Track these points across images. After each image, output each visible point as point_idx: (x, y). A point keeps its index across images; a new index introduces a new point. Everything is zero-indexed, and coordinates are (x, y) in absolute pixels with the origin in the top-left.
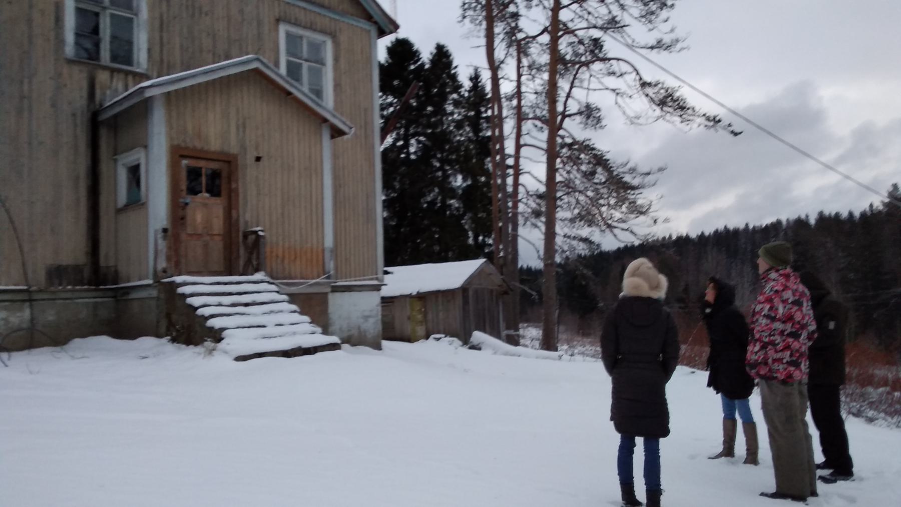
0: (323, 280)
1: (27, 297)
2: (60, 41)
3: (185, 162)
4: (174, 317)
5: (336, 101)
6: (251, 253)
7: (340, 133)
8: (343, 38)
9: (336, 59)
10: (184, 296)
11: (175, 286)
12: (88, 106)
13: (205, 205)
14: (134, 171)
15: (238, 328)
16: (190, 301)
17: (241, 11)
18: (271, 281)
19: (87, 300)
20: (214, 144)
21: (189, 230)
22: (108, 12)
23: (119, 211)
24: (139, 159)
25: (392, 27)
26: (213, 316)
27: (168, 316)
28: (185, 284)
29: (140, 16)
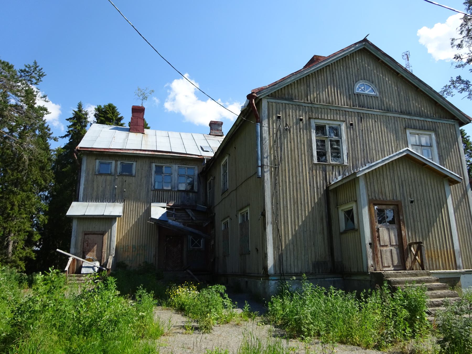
8: (440, 131)
9: (438, 143)
14: (349, 214)
19: (330, 279)
23: (341, 234)
24: (352, 207)
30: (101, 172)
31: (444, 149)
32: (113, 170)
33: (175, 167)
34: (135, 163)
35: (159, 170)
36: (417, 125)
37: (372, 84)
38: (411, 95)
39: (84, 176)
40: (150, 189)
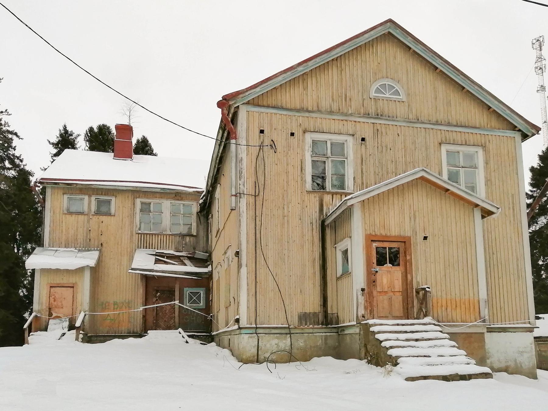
0: (480, 323)
1: (288, 331)
2: (303, 180)
3: (375, 245)
4: (369, 347)
5: (487, 193)
6: (422, 304)
7: (490, 213)
8: (491, 147)
9: (487, 163)
10: (374, 333)
11: (368, 326)
12: (320, 217)
13: (389, 272)
14: (345, 253)
15: (409, 356)
16: (378, 336)
17: (414, 143)
18: (437, 323)
19: (321, 334)
20: (394, 231)
21: (379, 289)
22: (330, 159)
25: (534, 131)
26: (391, 347)
27: (366, 346)
28: (375, 325)
29: (348, 158)
30: (71, 210)
31: (244, 151)
32: (86, 209)
33: (167, 205)
34: (113, 199)
35: (146, 208)
36: (479, 141)
37: (397, 83)
38: (455, 97)
39: (49, 216)
40: (134, 233)
